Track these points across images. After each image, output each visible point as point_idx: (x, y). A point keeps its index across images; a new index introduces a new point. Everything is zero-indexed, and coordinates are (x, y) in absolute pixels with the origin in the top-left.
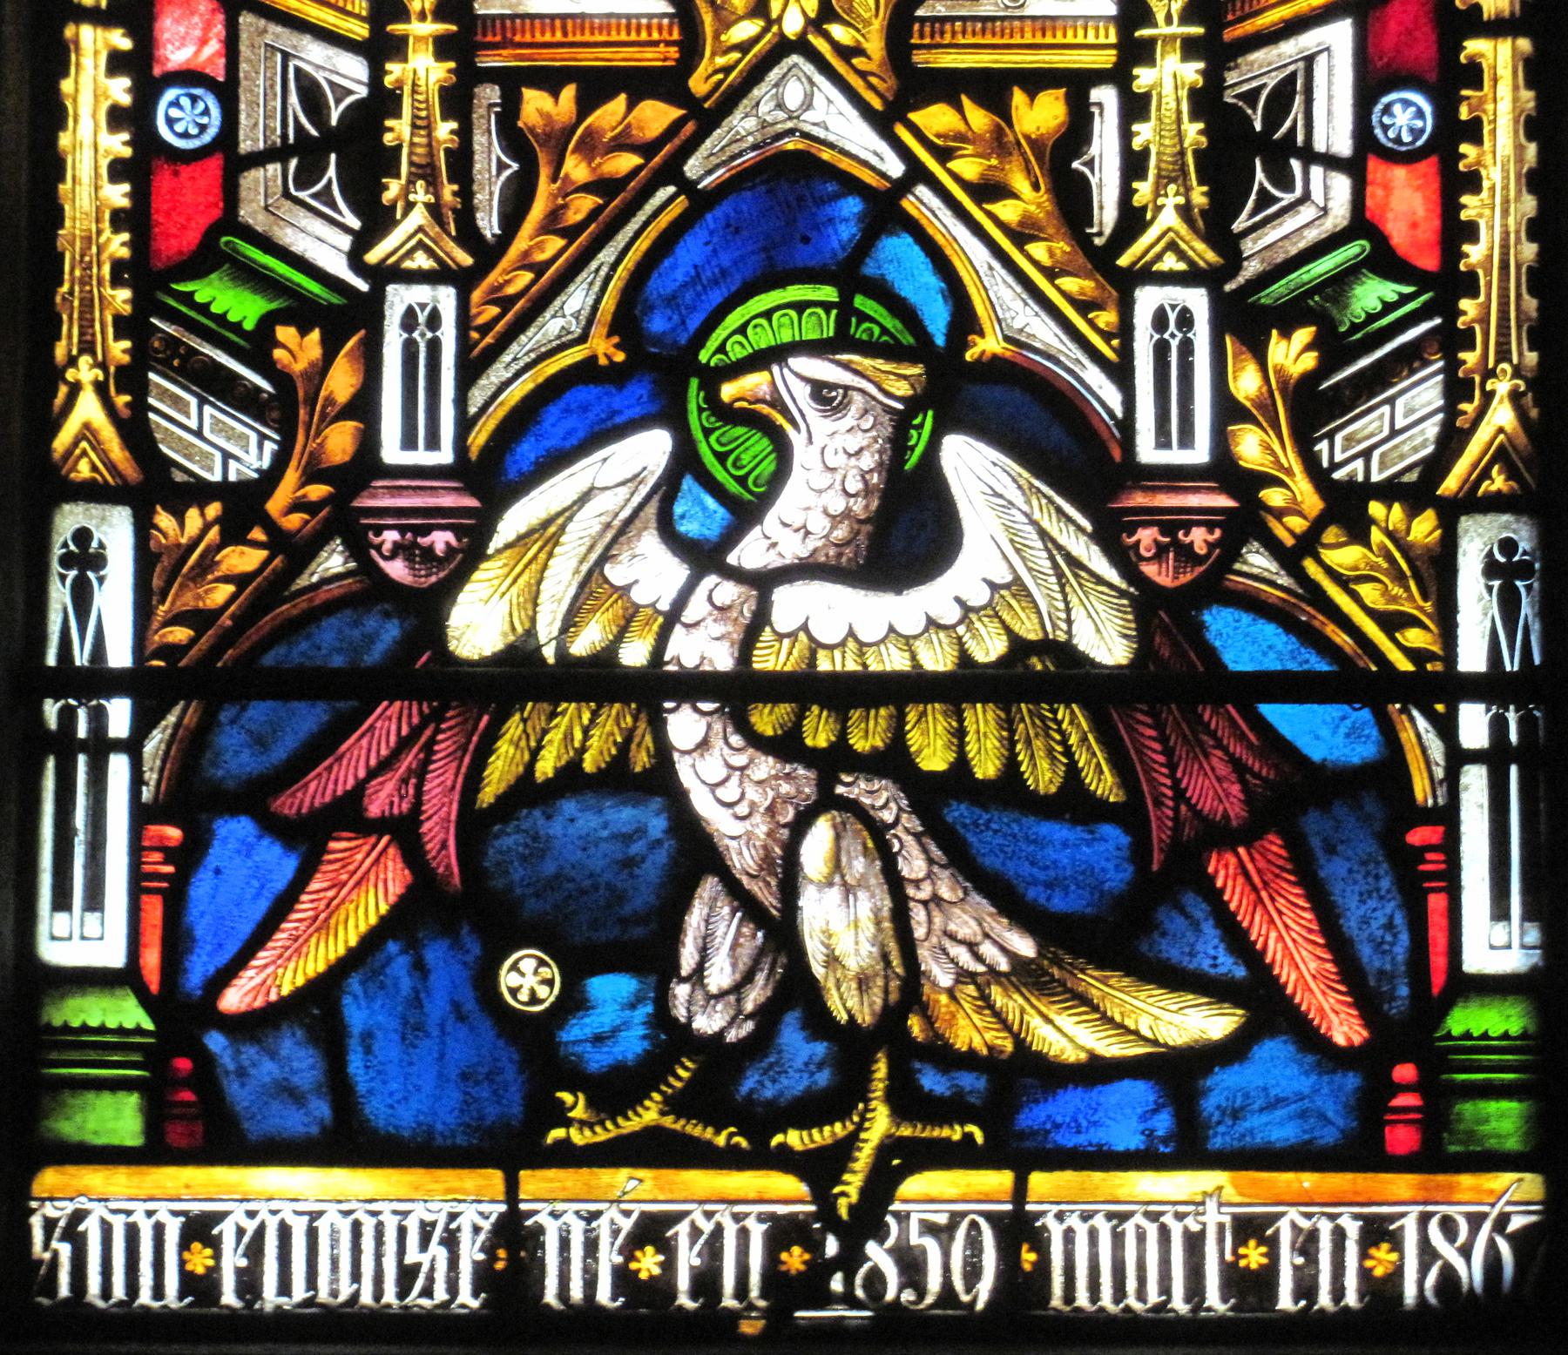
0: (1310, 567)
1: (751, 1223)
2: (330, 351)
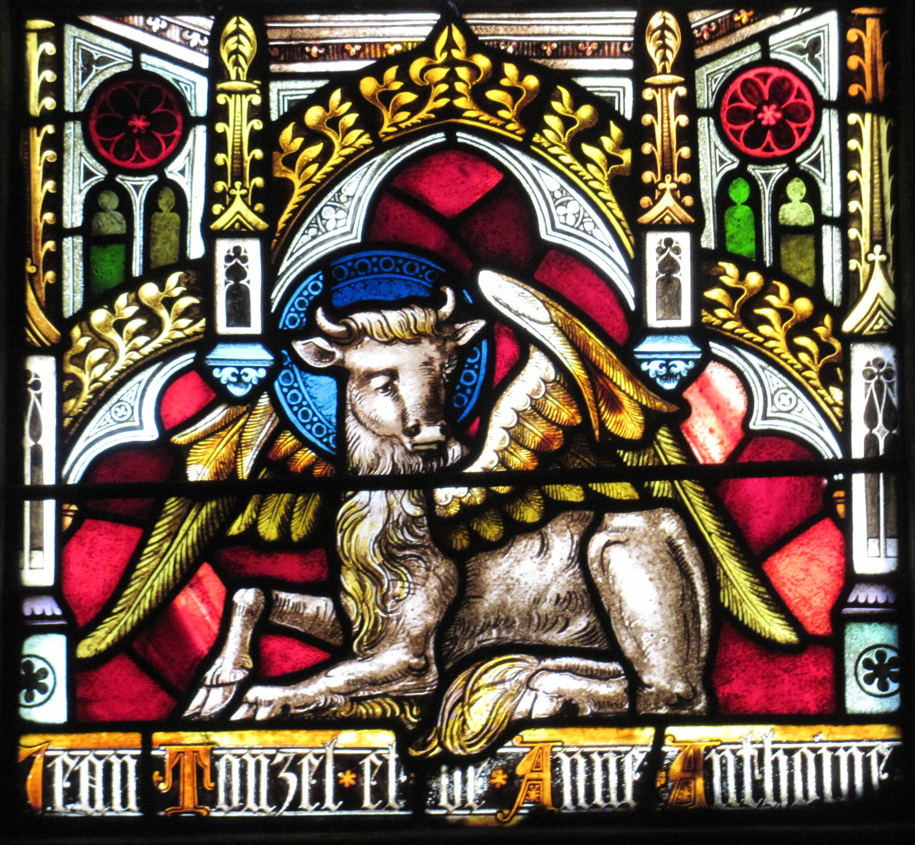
1: (127, 759)
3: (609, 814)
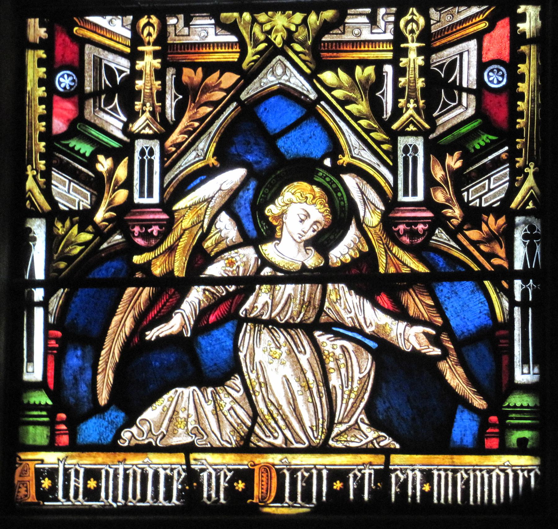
0: (460, 237)
2: (116, 164)
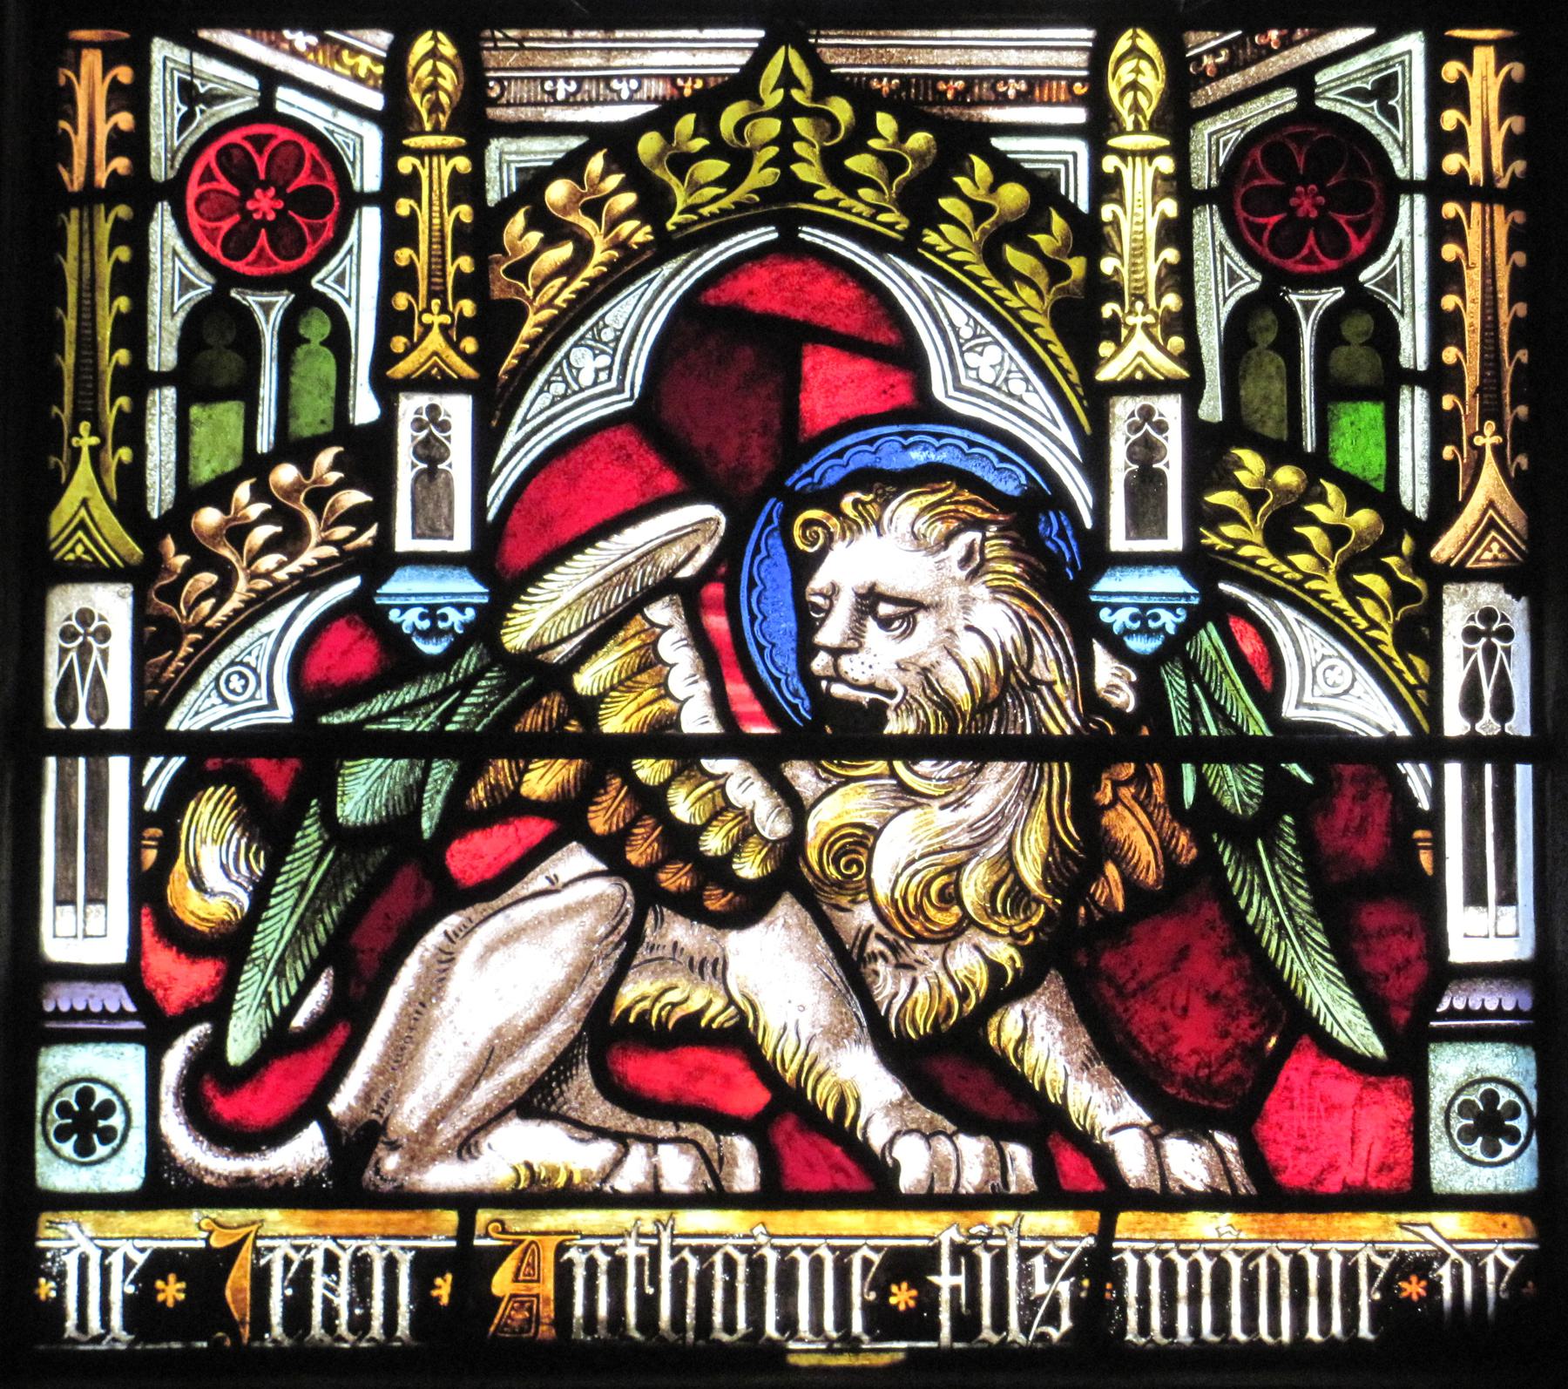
3: (1150, 1351)
